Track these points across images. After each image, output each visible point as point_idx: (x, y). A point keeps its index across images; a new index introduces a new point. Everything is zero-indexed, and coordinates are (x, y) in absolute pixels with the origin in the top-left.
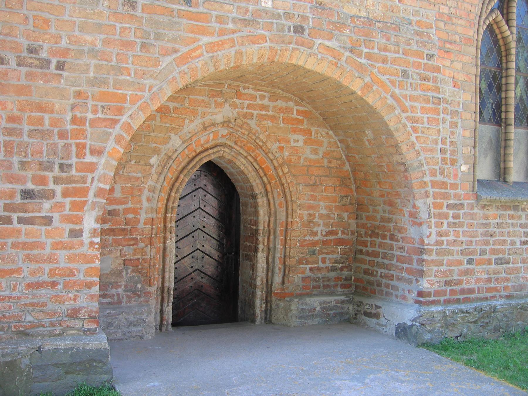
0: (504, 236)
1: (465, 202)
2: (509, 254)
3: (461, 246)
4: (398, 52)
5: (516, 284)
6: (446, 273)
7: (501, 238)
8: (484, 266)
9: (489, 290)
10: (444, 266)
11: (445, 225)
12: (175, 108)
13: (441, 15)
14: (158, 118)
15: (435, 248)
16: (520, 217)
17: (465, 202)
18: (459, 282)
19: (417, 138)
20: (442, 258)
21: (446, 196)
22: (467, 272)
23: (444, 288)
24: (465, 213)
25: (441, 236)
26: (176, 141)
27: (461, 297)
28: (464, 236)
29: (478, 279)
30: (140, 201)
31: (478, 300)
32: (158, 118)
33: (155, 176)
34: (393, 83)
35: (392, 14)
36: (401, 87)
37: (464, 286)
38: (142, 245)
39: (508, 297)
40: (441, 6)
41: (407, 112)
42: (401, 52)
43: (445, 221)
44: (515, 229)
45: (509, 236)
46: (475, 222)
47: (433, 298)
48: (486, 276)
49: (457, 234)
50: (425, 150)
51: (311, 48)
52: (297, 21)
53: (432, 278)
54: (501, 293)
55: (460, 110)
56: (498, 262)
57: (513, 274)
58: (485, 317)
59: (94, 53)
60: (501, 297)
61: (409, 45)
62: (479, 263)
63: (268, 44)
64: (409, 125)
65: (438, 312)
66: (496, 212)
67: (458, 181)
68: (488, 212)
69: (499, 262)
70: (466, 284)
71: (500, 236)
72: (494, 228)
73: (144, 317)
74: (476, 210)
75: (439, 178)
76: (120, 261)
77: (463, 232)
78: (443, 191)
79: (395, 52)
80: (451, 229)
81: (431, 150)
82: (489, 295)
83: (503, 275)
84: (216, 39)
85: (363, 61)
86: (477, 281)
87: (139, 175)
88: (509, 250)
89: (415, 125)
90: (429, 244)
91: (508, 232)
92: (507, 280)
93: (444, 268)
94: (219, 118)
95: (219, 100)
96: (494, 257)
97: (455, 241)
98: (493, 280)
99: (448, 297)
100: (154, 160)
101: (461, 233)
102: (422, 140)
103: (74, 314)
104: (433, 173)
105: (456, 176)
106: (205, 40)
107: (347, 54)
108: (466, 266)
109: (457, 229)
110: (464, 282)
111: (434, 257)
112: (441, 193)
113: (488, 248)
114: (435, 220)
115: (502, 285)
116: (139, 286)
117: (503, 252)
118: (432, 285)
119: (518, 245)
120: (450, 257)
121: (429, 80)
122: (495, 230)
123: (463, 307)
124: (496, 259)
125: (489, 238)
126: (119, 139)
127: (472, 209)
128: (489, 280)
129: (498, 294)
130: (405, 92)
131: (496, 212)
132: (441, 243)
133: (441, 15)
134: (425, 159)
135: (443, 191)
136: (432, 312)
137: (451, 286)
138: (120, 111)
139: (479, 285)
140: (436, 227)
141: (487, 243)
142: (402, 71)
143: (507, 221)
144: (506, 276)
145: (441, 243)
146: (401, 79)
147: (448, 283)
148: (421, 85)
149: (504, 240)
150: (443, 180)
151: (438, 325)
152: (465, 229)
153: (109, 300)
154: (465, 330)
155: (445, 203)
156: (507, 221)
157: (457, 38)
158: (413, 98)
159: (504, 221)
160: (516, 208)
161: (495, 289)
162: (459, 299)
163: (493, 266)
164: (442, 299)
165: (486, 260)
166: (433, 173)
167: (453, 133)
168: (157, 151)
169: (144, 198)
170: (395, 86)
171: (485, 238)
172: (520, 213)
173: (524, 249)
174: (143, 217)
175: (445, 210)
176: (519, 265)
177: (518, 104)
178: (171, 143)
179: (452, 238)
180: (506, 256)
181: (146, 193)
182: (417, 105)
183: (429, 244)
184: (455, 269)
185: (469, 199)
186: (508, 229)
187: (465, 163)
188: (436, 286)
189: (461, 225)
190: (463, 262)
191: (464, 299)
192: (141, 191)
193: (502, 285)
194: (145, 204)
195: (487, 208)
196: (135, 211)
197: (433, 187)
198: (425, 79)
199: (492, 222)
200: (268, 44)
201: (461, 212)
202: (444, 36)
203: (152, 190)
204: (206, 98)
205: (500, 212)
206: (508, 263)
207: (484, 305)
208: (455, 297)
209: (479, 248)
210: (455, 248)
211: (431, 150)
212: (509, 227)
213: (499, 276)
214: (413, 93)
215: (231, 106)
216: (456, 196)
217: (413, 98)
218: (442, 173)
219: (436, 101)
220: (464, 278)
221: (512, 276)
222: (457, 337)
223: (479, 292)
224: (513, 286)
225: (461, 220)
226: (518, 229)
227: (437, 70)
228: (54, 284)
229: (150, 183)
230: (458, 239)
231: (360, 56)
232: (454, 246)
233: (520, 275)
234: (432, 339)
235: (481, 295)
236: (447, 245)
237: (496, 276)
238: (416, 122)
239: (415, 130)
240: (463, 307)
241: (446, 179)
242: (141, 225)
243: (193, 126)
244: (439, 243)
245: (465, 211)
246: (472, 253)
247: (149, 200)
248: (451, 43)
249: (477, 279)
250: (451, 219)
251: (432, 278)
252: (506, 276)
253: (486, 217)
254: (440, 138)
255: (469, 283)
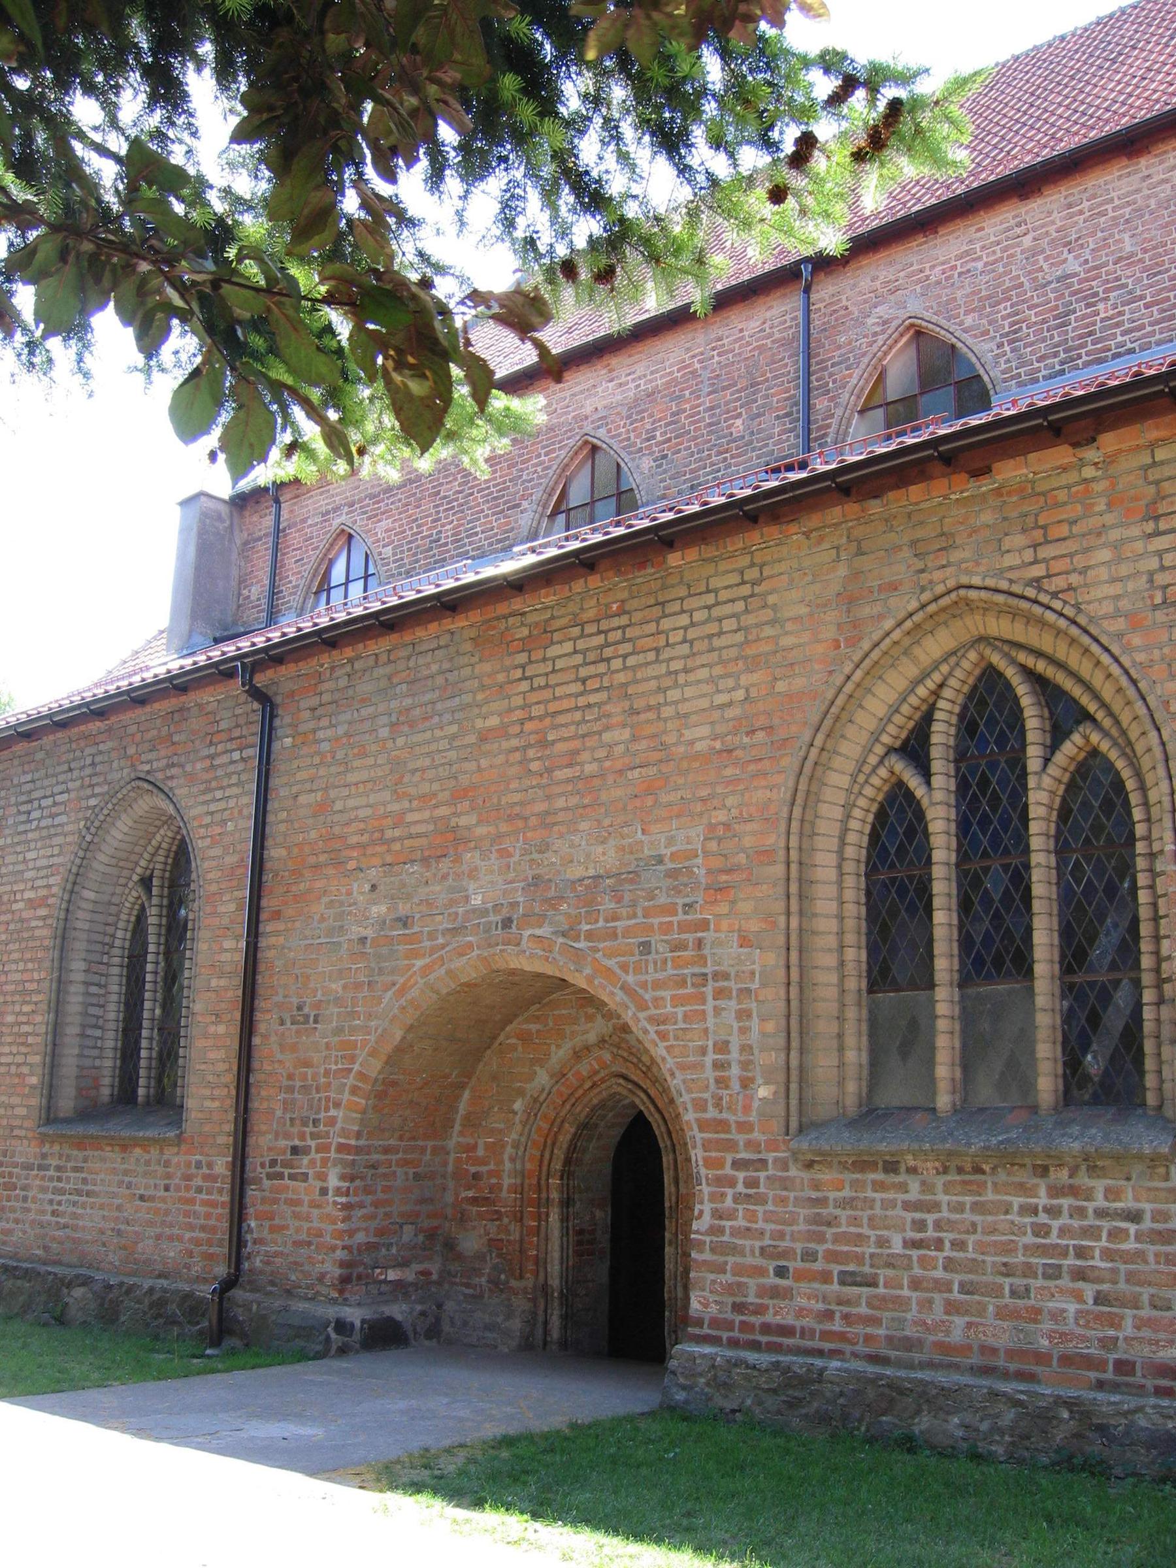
0: (861, 1226)
1: (770, 1157)
2: (872, 1266)
3: (761, 1240)
4: (635, 916)
5: (899, 1334)
6: (730, 1289)
7: (852, 1229)
8: (816, 1285)
9: (826, 1335)
10: (728, 1275)
11: (729, 1199)
12: (538, 1031)
13: (711, 827)
14: (520, 1049)
15: (708, 1239)
16: (903, 1188)
17: (770, 1157)
18: (760, 1310)
19: (667, 1048)
20: (722, 1259)
21: (731, 1146)
22: (775, 1293)
23: (729, 1316)
24: (768, 1178)
25: (721, 1218)
26: (542, 1078)
27: (764, 1339)
28: (766, 1221)
29: (802, 1309)
30: (502, 1162)
31: (791, 1351)
32: (520, 1049)
33: (519, 1127)
34: (624, 967)
35: (632, 857)
36: (637, 970)
37: (769, 1318)
38: (506, 1220)
39: (874, 1359)
40: (714, 813)
41: (647, 1008)
42: (640, 914)
43: (730, 1192)
44: (889, 1213)
45: (873, 1227)
46: (792, 1195)
47: (706, 1330)
48: (820, 1306)
49: (752, 1217)
50: (683, 1067)
51: (518, 944)
52: (505, 912)
53: (706, 1294)
54: (857, 1348)
55: (755, 986)
56: (847, 1279)
57: (888, 1310)
58: (796, 1387)
59: (338, 1001)
60: (855, 1355)
61: (652, 899)
62: (800, 1276)
63: (476, 952)
64: (652, 1029)
65: (704, 1356)
66: (841, 1176)
67: (753, 1118)
68: (819, 1176)
69: (849, 1279)
70: (775, 1314)
71: (849, 1224)
72: (835, 1207)
73: (499, 1320)
74: (793, 1172)
75: (712, 1113)
76: (485, 1240)
77: (765, 1212)
78: (723, 1136)
79: (629, 918)
80: (740, 1207)
81: (694, 1067)
82: (827, 1346)
83: (863, 1310)
84: (428, 960)
85: (581, 945)
86: (800, 1312)
87: (502, 1126)
88: (872, 1256)
89: (662, 1027)
90: (697, 1232)
91: (870, 1219)
92: (875, 1321)
93: (727, 1278)
94: (592, 1038)
95: (591, 1011)
96: (836, 1269)
97: (748, 1229)
98: (838, 1315)
99: (736, 1334)
100: (518, 1105)
101: (760, 1215)
102: (677, 1051)
103: (321, 1278)
104: (700, 1106)
105: (747, 1109)
106: (419, 963)
107: (561, 940)
108: (772, 1280)
109: (751, 1207)
110: (771, 1311)
111: (707, 1256)
112: (718, 1141)
113: (821, 1248)
114: (710, 1189)
115: (859, 1330)
116: (503, 1277)
117: (859, 1259)
118: (706, 1306)
119: (897, 1247)
120: (739, 1259)
121: (685, 948)
122: (838, 1212)
123: (751, 1357)
124: (841, 1273)
125: (824, 1228)
126: (354, 1090)
127: (786, 1168)
128: (829, 1315)
129: (848, 1348)
130: (643, 978)
131: (841, 1176)
132: (720, 1231)
133: (711, 827)
134: (684, 1081)
135: (723, 1136)
136: (691, 1354)
137: (743, 1314)
138: (353, 1060)
139: (807, 1322)
140: (711, 1201)
141: (821, 1238)
142: (641, 944)
143: (870, 1194)
144: (870, 1312)
145: (720, 1231)
146: (637, 958)
147: (738, 1308)
148: (673, 959)
149: (859, 1235)
150: (719, 1116)
151: (703, 1380)
152: (770, 1207)
153: (471, 1291)
154: (749, 1402)
155: (729, 1159)
156: (870, 1194)
157: (742, 858)
158: (657, 985)
159: (862, 1195)
160: (891, 1167)
161: (842, 1337)
162: (759, 1343)
163: (835, 1287)
164: (725, 1335)
165: (818, 1272)
166: (700, 1106)
167: (743, 1031)
168: (521, 1093)
169: (506, 1157)
170: (627, 972)
171: (813, 1228)
172: (901, 1178)
173: (915, 1258)
174: (507, 1182)
175: (728, 1170)
176: (906, 1292)
177: (1069, 922)
178: (536, 1081)
179: (741, 1222)
180: (867, 1269)
181: (509, 1150)
182: (666, 994)
183: (697, 1232)
184: (752, 1283)
185: (776, 1150)
186: (870, 1212)
187: (766, 1083)
188: (713, 1309)
189: (761, 1200)
190: (767, 1270)
191: (768, 1343)
192: (503, 1147)
193: (859, 1330)
194: (508, 1165)
195: (817, 1167)
196: (497, 1174)
197: (701, 1130)
198: (680, 946)
199: (832, 1195)
200: (476, 952)
201: (762, 1175)
202: (717, 863)
203: (516, 1146)
204: (573, 1012)
205: (849, 1176)
206: (874, 1284)
207: (798, 1363)
208: (751, 1337)
209: (799, 1247)
210: (748, 1243)
211: (694, 1067)
212: (872, 1208)
213: (854, 1310)
214: (661, 975)
215: (603, 1016)
216: (749, 1144)
217: (657, 985)
218: (718, 1105)
219: (699, 980)
220: (771, 1302)
221: (887, 1314)
222: (734, 1411)
223: (802, 1336)
224: (889, 1339)
225: (762, 1190)
226: (898, 1211)
227: (704, 925)
228: (309, 1244)
229: (514, 1136)
230: (754, 1226)
231: (577, 939)
232: (744, 1237)
233: (909, 1316)
234: (686, 1402)
235: (809, 1344)
236: (732, 1234)
237: (846, 1309)
238: (664, 1023)
239: (663, 1036)
240: (751, 1357)
241: (724, 1115)
242: (504, 1194)
243: (561, 1052)
244: (715, 1231)
245: (770, 1172)
246: (786, 1254)
247: (513, 1160)
248: (729, 871)
249: (801, 1306)
250: (740, 1188)
251: (706, 1294)
252: (870, 1312)
253: (816, 1186)
254: (710, 1043)
255: (779, 1314)
